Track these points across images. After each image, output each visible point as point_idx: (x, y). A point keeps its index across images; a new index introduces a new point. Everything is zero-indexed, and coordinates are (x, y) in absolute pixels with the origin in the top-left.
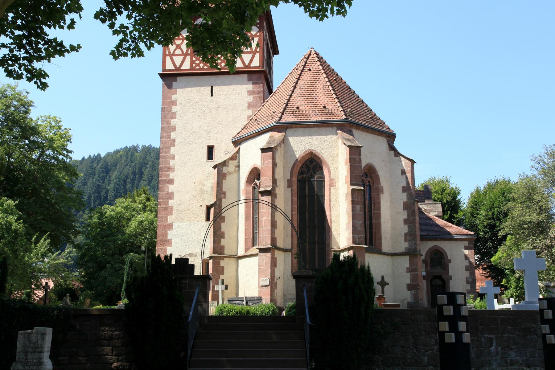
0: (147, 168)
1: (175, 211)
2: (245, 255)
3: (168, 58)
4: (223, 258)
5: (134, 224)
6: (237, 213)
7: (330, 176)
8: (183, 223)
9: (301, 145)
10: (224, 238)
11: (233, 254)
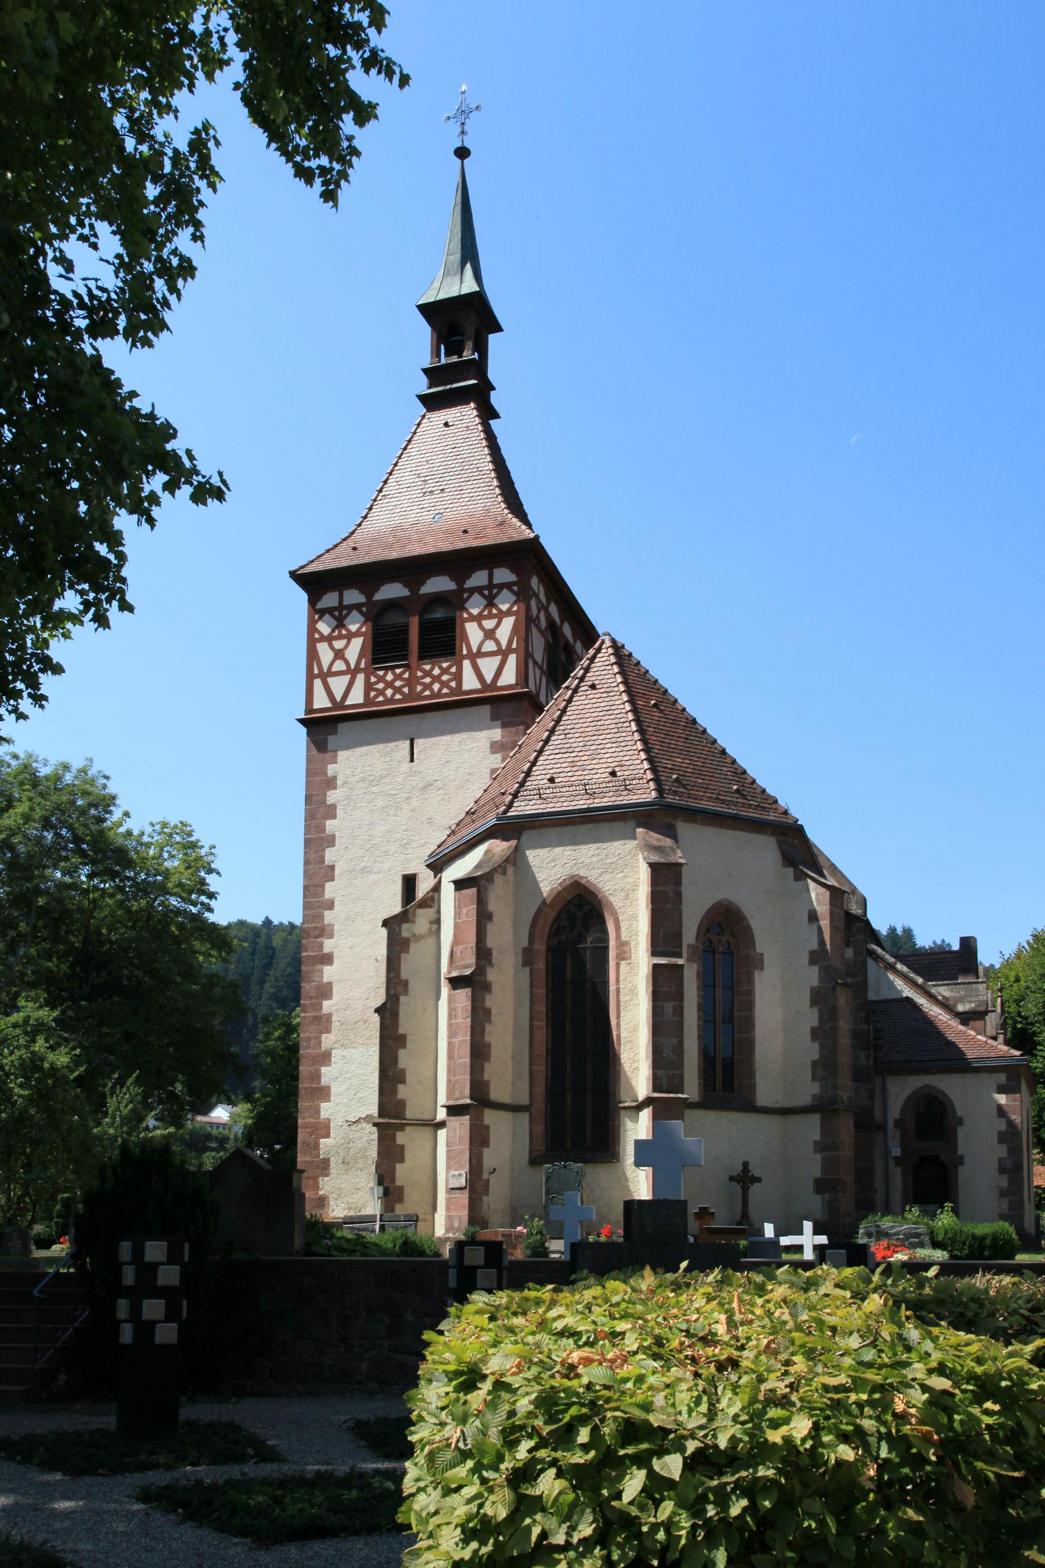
1: (335, 1024)
3: (318, 683)
4: (401, 1128)
7: (618, 936)
8: (352, 1051)
9: (551, 866)
11: (426, 1117)
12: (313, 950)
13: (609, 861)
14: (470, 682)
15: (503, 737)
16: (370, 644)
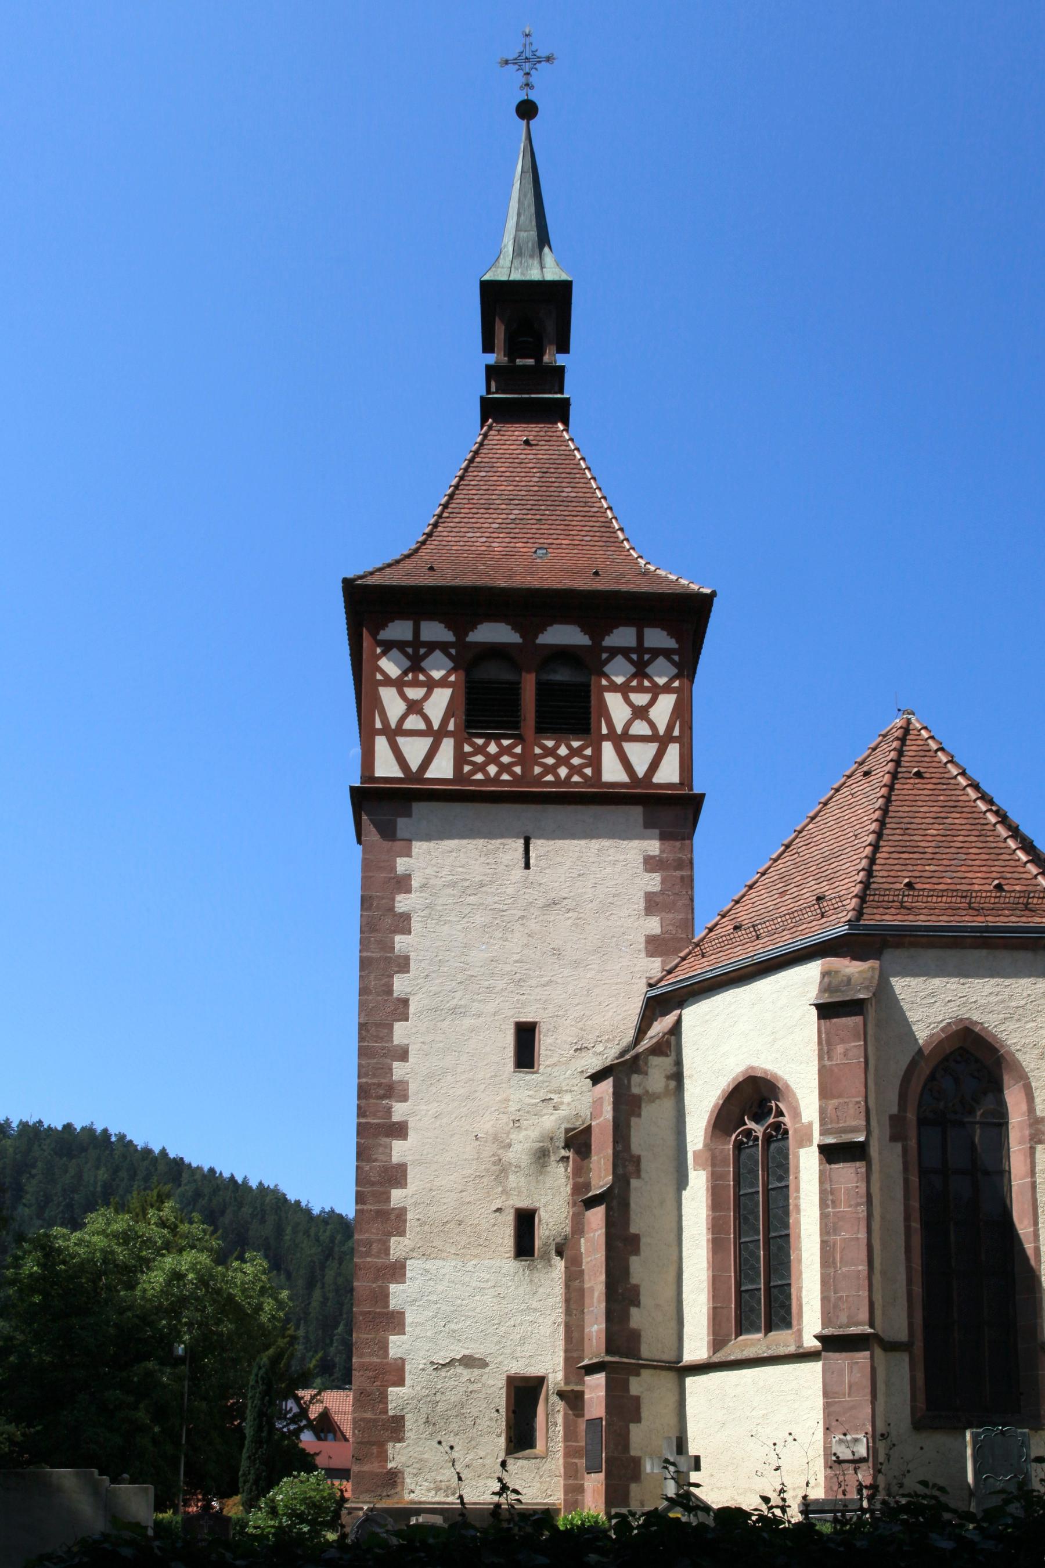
0: (33, 1176)
2: (716, 1359)
3: (381, 744)
5: (153, 1281)
6: (674, 1225)
8: (441, 1263)
9: (931, 1003)
10: (638, 1304)
11: (666, 1357)
12: (374, 1115)
13: (1013, 1004)
14: (612, 772)
15: (662, 851)
16: (462, 700)
